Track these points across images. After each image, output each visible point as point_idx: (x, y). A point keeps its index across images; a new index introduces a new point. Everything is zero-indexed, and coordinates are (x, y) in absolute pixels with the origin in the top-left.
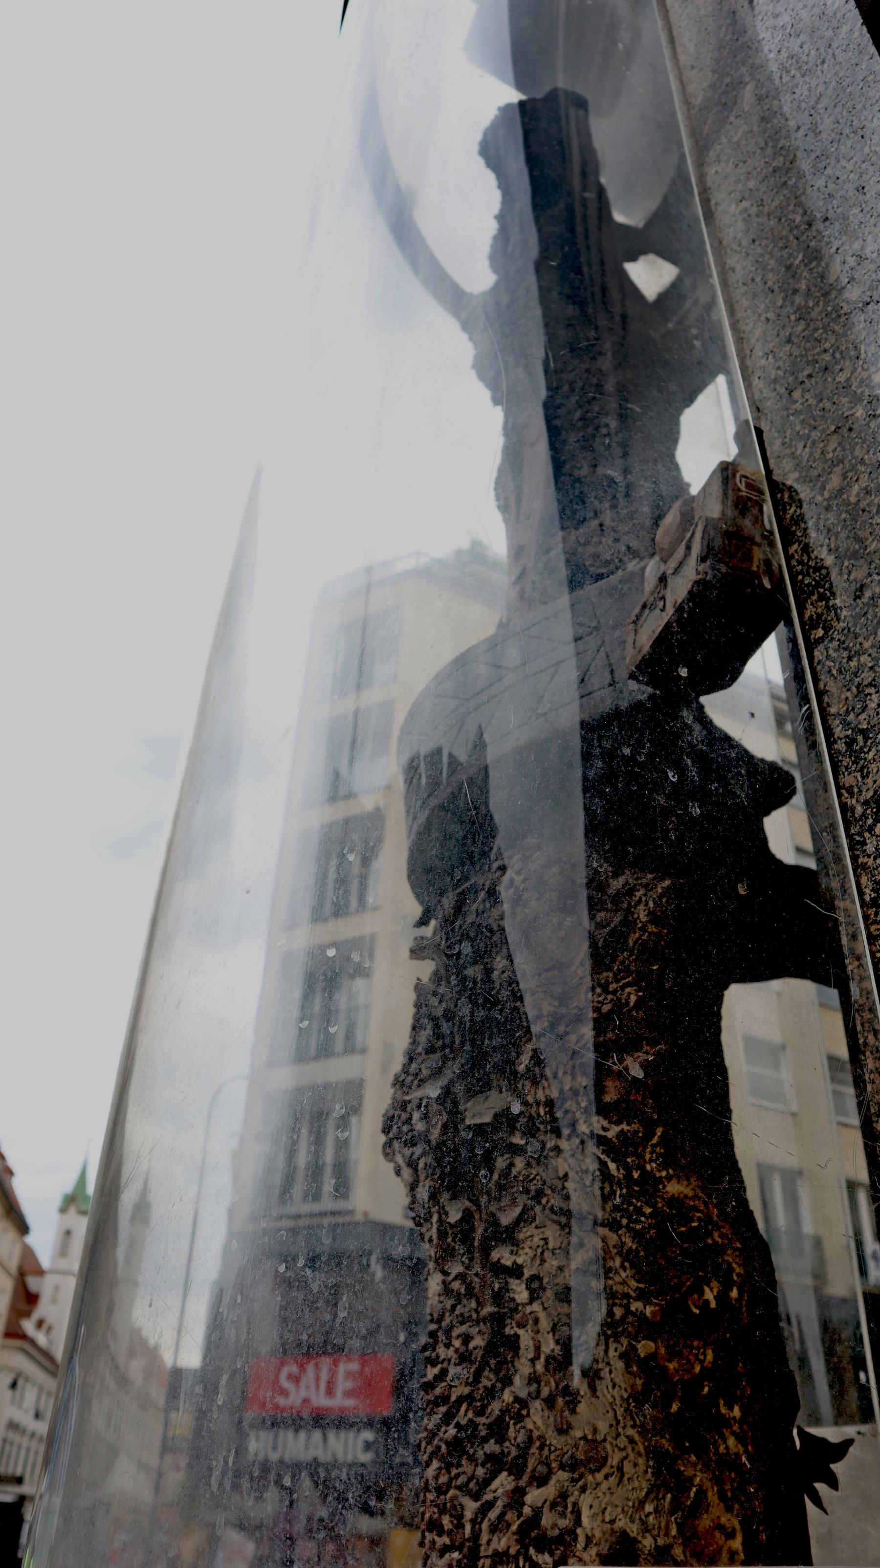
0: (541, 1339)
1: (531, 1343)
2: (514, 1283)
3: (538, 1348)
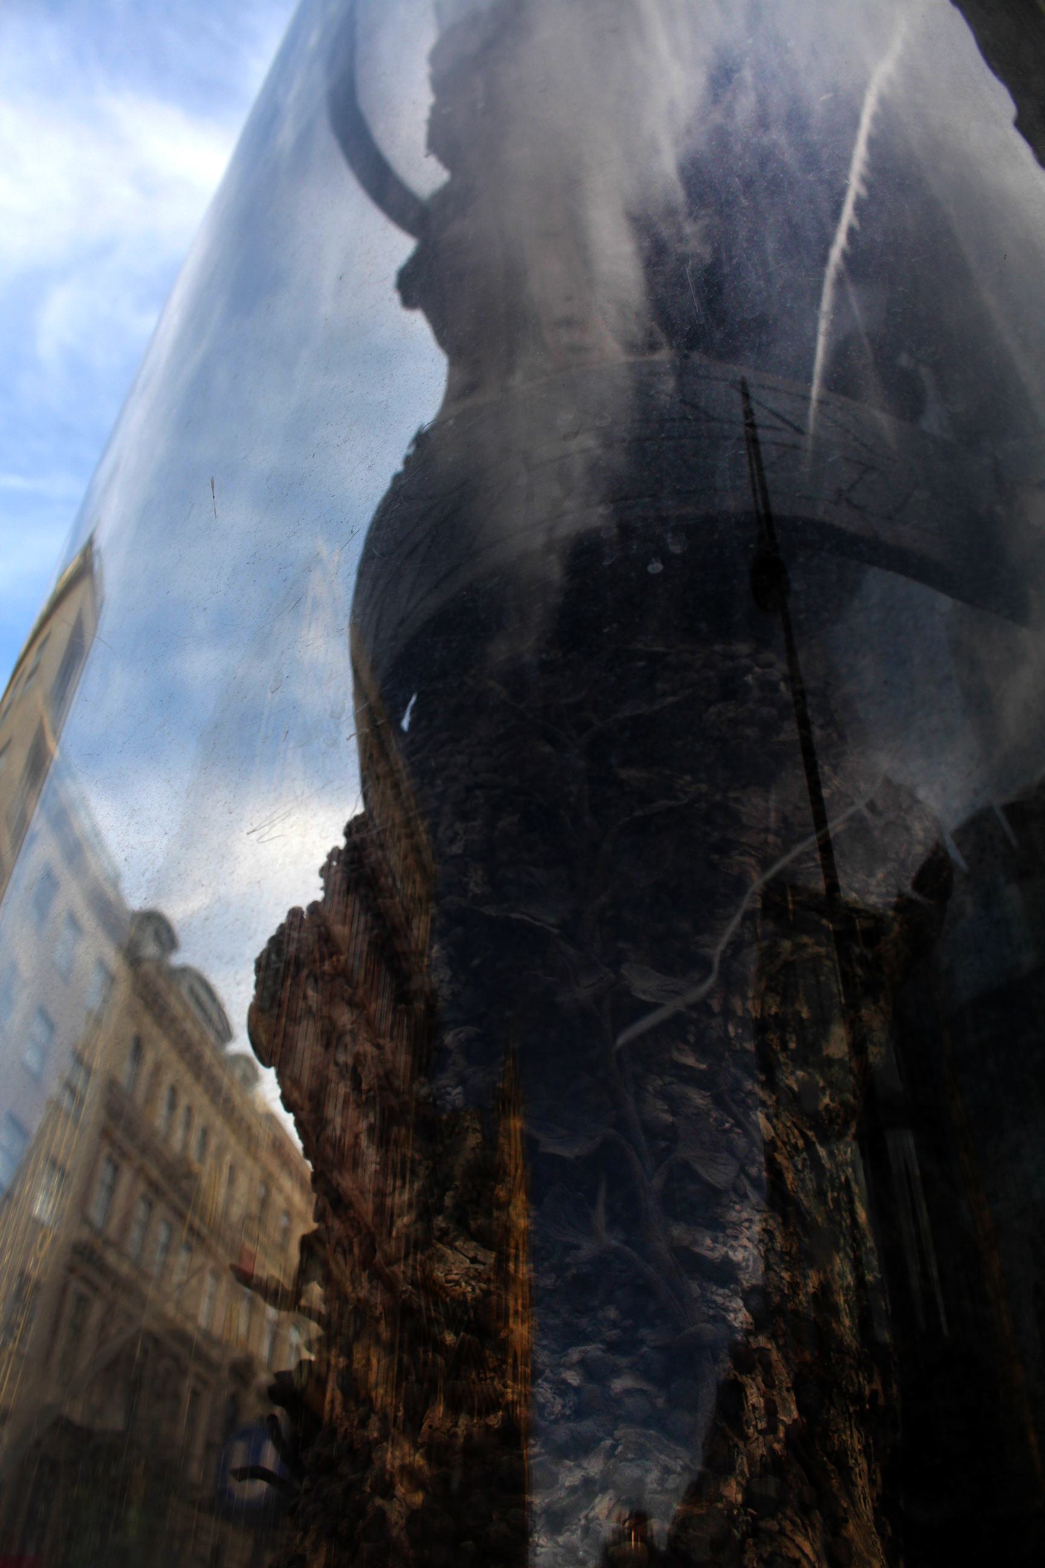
0: (777, 1399)
1: (761, 1402)
2: (719, 1295)
3: (771, 1411)
